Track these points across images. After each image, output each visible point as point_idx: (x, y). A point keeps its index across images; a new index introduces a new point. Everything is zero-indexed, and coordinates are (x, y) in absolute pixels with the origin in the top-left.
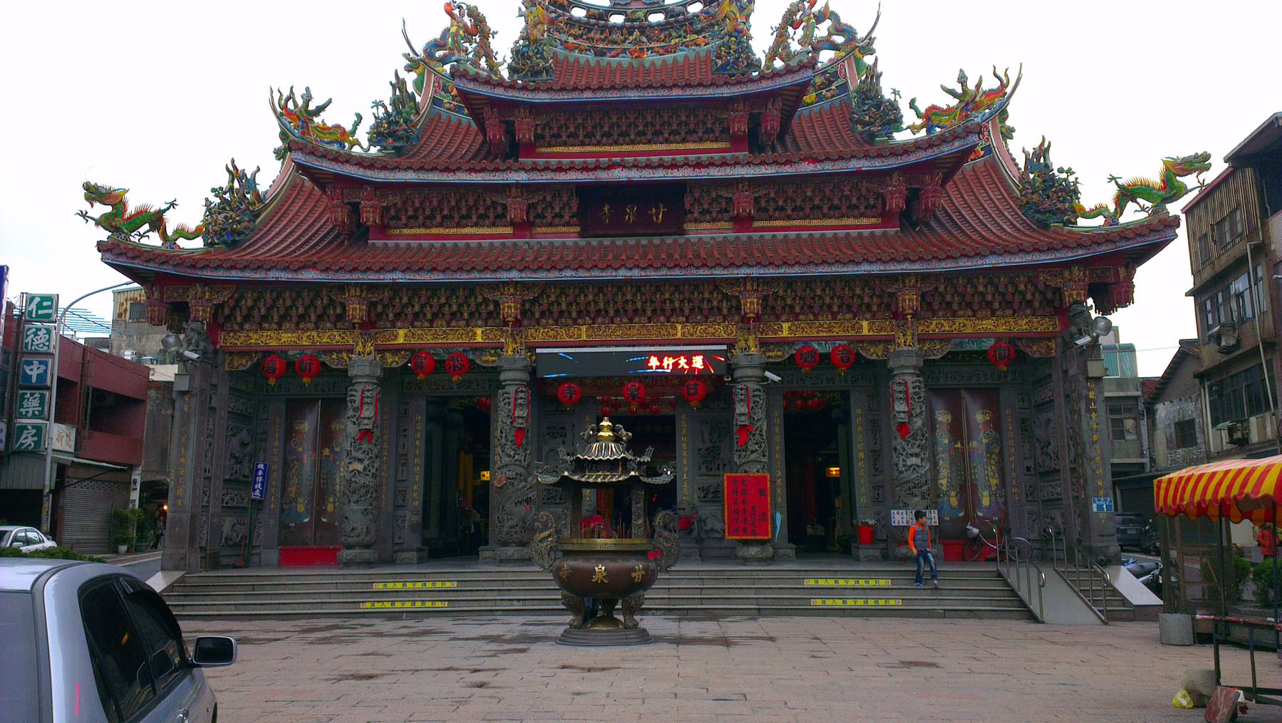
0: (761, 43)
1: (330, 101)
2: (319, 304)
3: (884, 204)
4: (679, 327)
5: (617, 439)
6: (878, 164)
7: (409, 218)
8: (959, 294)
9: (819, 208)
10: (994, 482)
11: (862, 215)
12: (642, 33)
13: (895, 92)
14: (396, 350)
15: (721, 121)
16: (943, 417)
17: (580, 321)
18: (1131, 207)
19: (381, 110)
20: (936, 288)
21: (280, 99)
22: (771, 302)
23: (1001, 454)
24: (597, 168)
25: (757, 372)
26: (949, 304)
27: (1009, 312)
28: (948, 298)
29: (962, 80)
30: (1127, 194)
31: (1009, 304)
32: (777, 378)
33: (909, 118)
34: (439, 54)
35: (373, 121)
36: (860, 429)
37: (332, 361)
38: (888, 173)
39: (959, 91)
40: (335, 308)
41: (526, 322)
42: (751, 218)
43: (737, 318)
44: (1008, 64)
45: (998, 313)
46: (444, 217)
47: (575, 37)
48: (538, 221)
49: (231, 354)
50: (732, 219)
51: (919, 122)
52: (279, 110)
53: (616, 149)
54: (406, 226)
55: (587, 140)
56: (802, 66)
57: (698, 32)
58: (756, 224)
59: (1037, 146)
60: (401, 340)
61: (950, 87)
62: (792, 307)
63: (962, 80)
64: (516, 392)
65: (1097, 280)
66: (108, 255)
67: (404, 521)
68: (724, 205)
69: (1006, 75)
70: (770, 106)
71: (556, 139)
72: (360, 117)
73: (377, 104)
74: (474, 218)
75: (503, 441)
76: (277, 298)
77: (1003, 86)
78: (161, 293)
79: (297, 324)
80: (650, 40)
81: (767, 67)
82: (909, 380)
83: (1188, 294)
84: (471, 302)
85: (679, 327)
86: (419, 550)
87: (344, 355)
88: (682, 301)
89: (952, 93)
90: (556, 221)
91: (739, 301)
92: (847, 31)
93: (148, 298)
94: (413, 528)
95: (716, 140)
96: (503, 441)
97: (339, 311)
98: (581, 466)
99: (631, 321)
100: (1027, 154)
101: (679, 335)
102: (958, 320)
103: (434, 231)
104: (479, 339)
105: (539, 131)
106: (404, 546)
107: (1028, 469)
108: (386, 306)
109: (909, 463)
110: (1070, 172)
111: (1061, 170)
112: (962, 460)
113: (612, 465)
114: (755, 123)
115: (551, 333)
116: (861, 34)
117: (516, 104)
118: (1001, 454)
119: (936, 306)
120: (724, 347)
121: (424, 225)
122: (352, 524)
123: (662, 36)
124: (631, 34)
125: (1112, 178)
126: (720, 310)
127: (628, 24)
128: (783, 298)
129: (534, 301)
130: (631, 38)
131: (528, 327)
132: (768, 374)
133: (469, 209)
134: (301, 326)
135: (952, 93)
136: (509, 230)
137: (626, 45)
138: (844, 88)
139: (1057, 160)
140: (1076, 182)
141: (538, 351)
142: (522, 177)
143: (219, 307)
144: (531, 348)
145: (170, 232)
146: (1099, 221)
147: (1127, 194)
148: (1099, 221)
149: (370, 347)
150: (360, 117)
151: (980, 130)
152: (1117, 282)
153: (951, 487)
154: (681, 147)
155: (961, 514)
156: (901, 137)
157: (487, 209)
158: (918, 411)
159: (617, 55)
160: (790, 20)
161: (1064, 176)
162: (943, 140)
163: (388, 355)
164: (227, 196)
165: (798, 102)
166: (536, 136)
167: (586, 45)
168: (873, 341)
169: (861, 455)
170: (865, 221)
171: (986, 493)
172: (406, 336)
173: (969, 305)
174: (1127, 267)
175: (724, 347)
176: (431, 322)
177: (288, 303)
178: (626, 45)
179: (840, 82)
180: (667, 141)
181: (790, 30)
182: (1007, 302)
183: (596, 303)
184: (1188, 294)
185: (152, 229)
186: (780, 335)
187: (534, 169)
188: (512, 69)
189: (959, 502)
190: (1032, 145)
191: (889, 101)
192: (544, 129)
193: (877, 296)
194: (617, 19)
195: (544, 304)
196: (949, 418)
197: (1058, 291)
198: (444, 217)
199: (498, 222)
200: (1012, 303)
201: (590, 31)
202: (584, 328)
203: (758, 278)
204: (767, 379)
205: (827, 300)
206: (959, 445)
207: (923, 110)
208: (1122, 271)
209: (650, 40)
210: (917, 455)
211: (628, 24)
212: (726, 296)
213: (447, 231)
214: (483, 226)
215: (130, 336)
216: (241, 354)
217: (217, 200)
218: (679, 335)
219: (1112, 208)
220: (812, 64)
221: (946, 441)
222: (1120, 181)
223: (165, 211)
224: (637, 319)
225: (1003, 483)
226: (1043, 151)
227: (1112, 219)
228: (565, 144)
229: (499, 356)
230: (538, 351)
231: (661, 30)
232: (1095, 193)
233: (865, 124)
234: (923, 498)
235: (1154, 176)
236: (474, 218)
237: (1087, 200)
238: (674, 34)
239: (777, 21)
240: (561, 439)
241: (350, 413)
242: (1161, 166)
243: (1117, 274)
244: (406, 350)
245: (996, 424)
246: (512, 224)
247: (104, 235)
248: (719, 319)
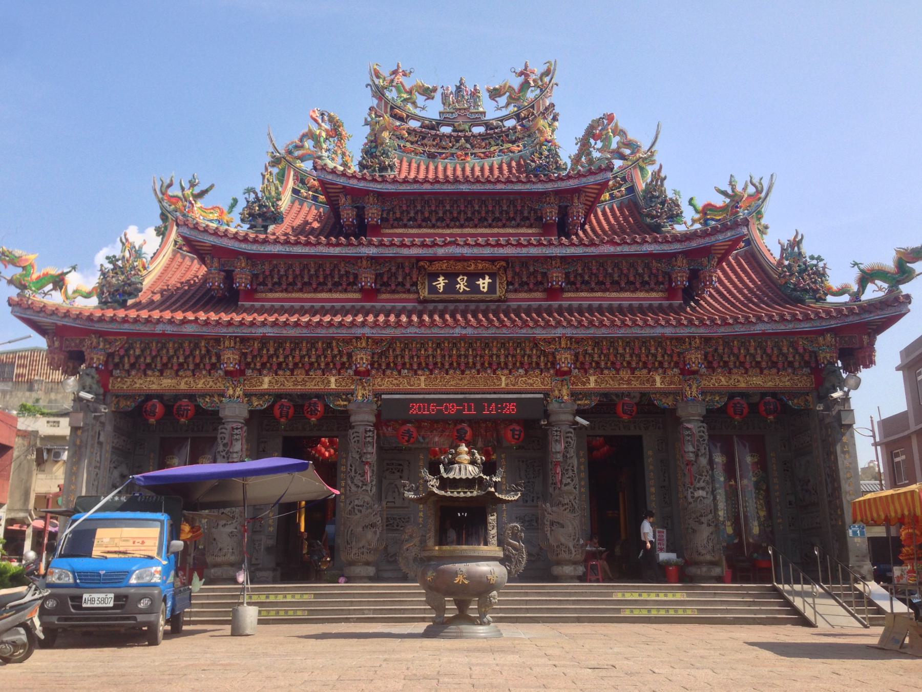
0: (567, 152)
1: (212, 186)
2: (199, 352)
3: (670, 281)
4: (503, 378)
5: (473, 462)
6: (666, 248)
7: (274, 284)
8: (734, 355)
9: (618, 283)
10: (762, 514)
11: (652, 290)
12: (467, 141)
13: (675, 192)
14: (261, 395)
15: (535, 211)
16: (719, 459)
17: (420, 372)
18: (870, 287)
19: (253, 195)
20: (716, 350)
21: (162, 186)
22: (581, 358)
23: (767, 491)
24: (434, 245)
25: (570, 418)
26: (726, 363)
27: (774, 371)
28: (726, 359)
29: (732, 184)
30: (866, 277)
31: (774, 364)
32: (585, 422)
33: (688, 214)
34: (296, 154)
35: (245, 204)
36: (651, 467)
37: (205, 403)
38: (674, 255)
39: (730, 192)
40: (210, 358)
41: (374, 372)
42: (562, 290)
43: (552, 371)
44: (761, 174)
45: (765, 372)
46: (304, 284)
47: (412, 143)
48: (383, 288)
49: (117, 396)
50: (545, 290)
51: (697, 216)
52: (160, 196)
53: (448, 231)
54: (271, 291)
55: (424, 224)
56: (601, 170)
57: (513, 142)
58: (566, 295)
59: (792, 238)
60: (265, 386)
61: (723, 189)
62: (598, 363)
63: (732, 184)
64: (366, 431)
65: (846, 346)
66: (17, 309)
67: (260, 545)
68: (539, 279)
69: (761, 183)
70: (576, 201)
71: (399, 222)
72: (235, 201)
73: (250, 190)
74: (330, 285)
75: (353, 474)
76: (162, 349)
77: (759, 192)
78: (61, 343)
79: (177, 372)
80: (473, 147)
81: (573, 169)
82: (694, 426)
83: (898, 369)
84: (328, 353)
85: (503, 378)
86: (274, 570)
87: (216, 399)
88: (507, 357)
89: (725, 193)
90: (399, 288)
91: (555, 357)
92: (633, 146)
93: (49, 346)
94: (269, 549)
95: (531, 226)
96: (353, 474)
97: (214, 360)
98: (445, 484)
99: (463, 372)
100: (782, 246)
101: (503, 385)
102: (733, 377)
103: (294, 295)
104: (333, 386)
105: (385, 215)
106: (260, 566)
107: (790, 503)
108: (259, 353)
109: (696, 495)
110: (819, 259)
111: (812, 258)
112: (733, 495)
113: (469, 483)
114: (564, 213)
115: (395, 382)
116: (645, 146)
117: (367, 192)
118: (767, 491)
119: (715, 365)
120: (541, 396)
121: (286, 291)
122: (220, 546)
123: (483, 144)
124: (457, 141)
125: (855, 264)
126: (538, 364)
127: (455, 134)
128: (591, 355)
129: (382, 354)
130: (458, 145)
131: (374, 377)
132: (578, 419)
133: (325, 277)
134: (180, 373)
135: (725, 193)
136: (357, 296)
137: (453, 151)
138: (631, 190)
139: (808, 249)
140: (824, 268)
141: (383, 396)
142: (372, 251)
143: (110, 356)
144: (377, 395)
145: (70, 292)
146: (845, 298)
147: (866, 277)
148: (845, 298)
149: (239, 392)
150: (235, 201)
151: (746, 223)
152: (862, 347)
153: (723, 523)
154: (502, 231)
155: (736, 541)
156: (680, 228)
157: (341, 277)
158: (703, 451)
159: (446, 158)
160: (591, 132)
161: (815, 262)
162: (715, 231)
163: (254, 399)
164: (120, 263)
165: (597, 200)
166: (382, 219)
167: (420, 149)
168: (665, 394)
169: (653, 490)
170: (654, 295)
171: (756, 523)
172: (270, 382)
173: (742, 364)
174: (869, 334)
175: (541, 396)
176: (292, 371)
177: (171, 352)
178: (453, 151)
179: (629, 185)
180: (490, 226)
181: (592, 141)
182: (773, 362)
183: (434, 357)
184: (898, 369)
185: (54, 289)
186: (588, 386)
187: (381, 244)
188: (362, 166)
189: (734, 530)
190: (787, 236)
191: (671, 199)
192: (388, 214)
193: (669, 354)
194: (446, 130)
195: (390, 355)
196: (725, 459)
197: (814, 354)
198: (304, 284)
199: (349, 288)
200: (777, 363)
201: (424, 138)
202: (423, 378)
203: (571, 338)
204: (577, 423)
205: (628, 358)
206: (733, 483)
207: (700, 206)
208: (865, 338)
209: (473, 147)
210: (703, 489)
211: (455, 134)
212: (543, 353)
213: (306, 296)
214: (336, 292)
215: (68, 367)
216: (127, 397)
217: (111, 266)
218: (503, 385)
219: (855, 288)
220: (610, 168)
221: (722, 479)
222: (862, 267)
223: (67, 273)
224: (467, 372)
225: (770, 515)
226: (796, 243)
227: (856, 296)
228: (405, 226)
229: (349, 401)
230: (383, 396)
231: (483, 140)
232: (840, 276)
233: (653, 217)
234: (709, 525)
235: (889, 262)
236: (330, 285)
237: (834, 281)
238: (493, 143)
239: (581, 133)
240: (398, 474)
241: (221, 448)
242: (894, 254)
243: (862, 341)
244: (270, 395)
245: (762, 465)
246: (362, 290)
247: (14, 292)
248: (537, 372)
